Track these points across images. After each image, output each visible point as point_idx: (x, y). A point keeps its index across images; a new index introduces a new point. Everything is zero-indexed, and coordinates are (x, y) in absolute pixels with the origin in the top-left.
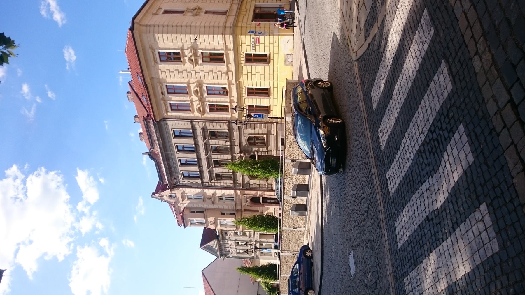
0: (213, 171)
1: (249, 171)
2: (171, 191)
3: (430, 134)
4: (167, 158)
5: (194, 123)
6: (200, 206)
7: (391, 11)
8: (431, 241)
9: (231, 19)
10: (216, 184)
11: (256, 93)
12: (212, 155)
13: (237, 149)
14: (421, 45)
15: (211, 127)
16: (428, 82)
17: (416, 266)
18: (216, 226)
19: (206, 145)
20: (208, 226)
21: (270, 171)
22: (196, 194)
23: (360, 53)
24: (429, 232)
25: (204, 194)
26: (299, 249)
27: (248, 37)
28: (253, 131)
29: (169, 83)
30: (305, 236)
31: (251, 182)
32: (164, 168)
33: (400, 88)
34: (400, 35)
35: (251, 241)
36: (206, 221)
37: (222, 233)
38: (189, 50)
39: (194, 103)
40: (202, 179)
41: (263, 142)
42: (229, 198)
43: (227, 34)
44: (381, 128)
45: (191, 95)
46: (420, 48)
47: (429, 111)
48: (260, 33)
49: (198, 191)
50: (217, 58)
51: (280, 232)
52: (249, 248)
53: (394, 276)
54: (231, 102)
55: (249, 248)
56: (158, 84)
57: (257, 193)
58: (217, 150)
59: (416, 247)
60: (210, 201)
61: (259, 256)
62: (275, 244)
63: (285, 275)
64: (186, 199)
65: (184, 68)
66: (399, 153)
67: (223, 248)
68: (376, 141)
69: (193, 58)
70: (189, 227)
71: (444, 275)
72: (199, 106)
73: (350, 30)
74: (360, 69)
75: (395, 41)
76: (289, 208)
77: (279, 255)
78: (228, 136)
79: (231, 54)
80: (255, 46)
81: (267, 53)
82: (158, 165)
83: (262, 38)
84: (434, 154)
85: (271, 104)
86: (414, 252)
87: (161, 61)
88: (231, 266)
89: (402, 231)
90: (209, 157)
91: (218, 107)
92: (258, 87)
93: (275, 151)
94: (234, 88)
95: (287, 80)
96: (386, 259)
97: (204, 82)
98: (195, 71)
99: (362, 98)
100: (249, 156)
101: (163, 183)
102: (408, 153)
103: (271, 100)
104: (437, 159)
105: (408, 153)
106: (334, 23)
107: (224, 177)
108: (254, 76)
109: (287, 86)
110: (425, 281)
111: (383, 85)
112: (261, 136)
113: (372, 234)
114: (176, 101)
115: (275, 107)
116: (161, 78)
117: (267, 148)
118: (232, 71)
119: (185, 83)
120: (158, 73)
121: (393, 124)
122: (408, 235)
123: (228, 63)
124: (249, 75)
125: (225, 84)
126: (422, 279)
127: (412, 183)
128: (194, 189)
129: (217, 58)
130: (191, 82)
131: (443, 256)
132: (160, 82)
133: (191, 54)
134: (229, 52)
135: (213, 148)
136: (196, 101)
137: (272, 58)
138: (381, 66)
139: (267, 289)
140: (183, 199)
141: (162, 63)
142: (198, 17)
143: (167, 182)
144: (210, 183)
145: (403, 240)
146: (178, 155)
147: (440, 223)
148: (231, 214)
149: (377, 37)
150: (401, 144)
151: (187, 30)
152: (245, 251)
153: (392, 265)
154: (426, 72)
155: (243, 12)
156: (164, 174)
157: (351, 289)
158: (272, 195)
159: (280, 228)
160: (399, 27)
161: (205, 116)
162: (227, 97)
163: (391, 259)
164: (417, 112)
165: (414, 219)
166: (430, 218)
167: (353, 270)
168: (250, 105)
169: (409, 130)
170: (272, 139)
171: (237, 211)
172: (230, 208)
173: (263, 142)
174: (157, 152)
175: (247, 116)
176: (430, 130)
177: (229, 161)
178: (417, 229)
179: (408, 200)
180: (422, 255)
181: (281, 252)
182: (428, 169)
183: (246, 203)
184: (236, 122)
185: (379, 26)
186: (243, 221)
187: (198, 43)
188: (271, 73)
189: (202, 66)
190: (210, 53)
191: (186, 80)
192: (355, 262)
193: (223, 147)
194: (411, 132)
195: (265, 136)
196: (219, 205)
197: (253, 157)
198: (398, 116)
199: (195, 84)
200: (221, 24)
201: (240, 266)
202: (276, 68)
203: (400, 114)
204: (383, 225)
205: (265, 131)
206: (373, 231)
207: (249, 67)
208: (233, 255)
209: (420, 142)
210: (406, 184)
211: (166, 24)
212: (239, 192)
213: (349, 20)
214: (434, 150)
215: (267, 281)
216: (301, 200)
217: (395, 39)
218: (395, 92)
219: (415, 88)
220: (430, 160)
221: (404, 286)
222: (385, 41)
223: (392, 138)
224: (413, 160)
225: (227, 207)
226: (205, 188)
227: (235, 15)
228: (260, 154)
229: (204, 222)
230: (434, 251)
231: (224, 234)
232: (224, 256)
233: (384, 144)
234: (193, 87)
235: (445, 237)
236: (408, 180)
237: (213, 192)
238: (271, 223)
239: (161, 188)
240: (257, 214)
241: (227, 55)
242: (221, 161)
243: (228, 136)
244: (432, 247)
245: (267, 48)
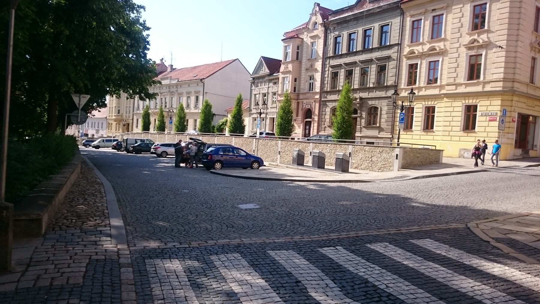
0: (341, 69)
1: (341, 107)
2: (321, 24)
3: (386, 294)
4: (357, 18)
5: (396, 48)
6: (304, 55)
7: (531, 269)
8: (277, 282)
9: (523, 89)
10: (327, 72)
11: (428, 116)
12: (359, 68)
13: (364, 95)
14: (489, 297)
15: (391, 67)
16: (445, 299)
17: (252, 265)
18: (283, 73)
19: (370, 61)
20: (284, 64)
21: (339, 130)
22: (317, 51)
23: (477, 231)
24: (285, 282)
25: (316, 60)
26: (259, 156)
27: (499, 108)
28: (384, 112)
29: (446, 17)
30: (272, 163)
31: (328, 110)
32: (346, 15)
33: (436, 270)
34: (501, 276)
35: (267, 108)
36: (289, 63)
37: (276, 79)
38: (487, 40)
39: (420, 47)
40: (332, 57)
41: (371, 123)
42: (311, 87)
43: (503, 84)
44: (389, 245)
45: (430, 43)
46: (486, 296)
47: (412, 296)
48: (502, 122)
49: (321, 53)
50: (474, 72)
51: (276, 138)
52: (261, 106)
53: (240, 244)
54: (420, 89)
55: (261, 106)
56: (445, 5)
57: (316, 116)
58: (364, 73)
59: (269, 268)
60: (309, 66)
61: (252, 116)
62: (264, 133)
63: (235, 142)
64: (312, 41)
65: (464, 34)
66: (364, 261)
67: (261, 80)
68: (377, 239)
69: (476, 44)
70: (282, 44)
71: (246, 291)
72: (416, 52)
73: (504, 222)
74: (456, 230)
75: (492, 270)
76: (300, 148)
77: (253, 136)
78: (380, 85)
79: (479, 89)
80: (486, 115)
81: (477, 129)
82: (351, 8)
83: (496, 124)
84: (365, 296)
85: (415, 133)
86: (264, 265)
87: (475, 6)
88: (243, 88)
89: (284, 256)
90: (357, 65)
91: (414, 73)
92: (436, 119)
93: (360, 135)
94: (436, 92)
95: (442, 151)
96: (256, 239)
97: (445, 58)
98: (460, 47)
99: (423, 229)
100: (357, 108)
101: (330, 15)
102: (364, 270)
103: (419, 133)
104: (360, 298)
105: (364, 270)
106: (513, 206)
107: (335, 80)
108: (449, 114)
109: (435, 150)
110: (238, 273)
111: (439, 252)
112: (378, 121)
113: (279, 228)
114: (424, 26)
115: (410, 137)
116: (453, 7)
117: (364, 127)
118: (456, 89)
119: (445, 35)
120: (459, 4)
121: (395, 258)
122: (280, 261)
123: (467, 85)
124: (451, 109)
125: (441, 82)
126: (240, 270)
127: (333, 270)
128: (322, 49)
129: (474, 72)
130: (445, 43)
131: (262, 292)
132: (448, 7)
133: (481, 41)
134: (481, 86)
135: (367, 69)
136: (423, 49)
137: (470, 134)
138: (462, 252)
139: (221, 124)
140: (311, 37)
141: (411, 22)
142: (529, 49)
143: (332, 19)
144: (328, 66)
145: (275, 256)
146: (360, 30)
147: (294, 293)
148: (295, 88)
149: (498, 251)
150: (374, 264)
151: (513, 36)
152: (264, 102)
153: (250, 244)
154: (456, 299)
155: (531, 102)
156: (339, 15)
157: (225, 204)
158: (314, 131)
159: (280, 138)
160: (511, 275)
161: (405, 59)
162: (426, 83)
163: (256, 243)
164: (410, 284)
165: (296, 269)
166: (299, 284)
167: (243, 206)
168: (415, 109)
169: (389, 274)
170: (374, 133)
171: (298, 95)
172: (301, 87)
173: (371, 123)
174: (365, 6)
175: (403, 106)
176: (390, 295)
177: (351, 86)
178: (287, 270)
179: (316, 265)
180: (262, 272)
181: (256, 139)
182: (349, 288)
183: (305, 104)
184: (396, 93)
185: (511, 254)
186: (288, 101)
187: (494, 50)
188: (451, 133)
189: (465, 55)
190: (481, 64)
191: (448, 37)
192: (250, 209)
193: (367, 79)
194: (387, 276)
195: (378, 125)
196: (304, 76)
197: (355, 112)
198: (404, 264)
199: (443, 47)
200: (517, 77)
201: (243, 97)
202: (457, 139)
203: (407, 267)
204: (288, 239)
205: (384, 125)
206: (282, 229)
207: (460, 109)
208: (253, 91)
209: (376, 283)
210: (332, 265)
211: (523, 10)
212: (317, 97)
213: (517, 222)
214: (368, 296)
215: (228, 124)
216: (309, 161)
217: (495, 270)
218: (431, 263)
219: (438, 285)
220: (358, 291)
221: (232, 252)
222: (492, 259)
223: (379, 255)
224: (357, 274)
225: (302, 84)
226: (323, 61)
227: (527, 93)
228: (358, 119)
229: (287, 60)
230: (267, 284)
231: (275, 81)
232: (253, 81)
233: (372, 247)
234: (439, 45)
235: (282, 296)
236: (336, 267)
237: (318, 69)
238: (285, 130)
239: (325, 13)
240: (294, 115)
241: (478, 84)
242: (352, 78)
243: (380, 85)
244: (271, 283)
245: (482, 129)
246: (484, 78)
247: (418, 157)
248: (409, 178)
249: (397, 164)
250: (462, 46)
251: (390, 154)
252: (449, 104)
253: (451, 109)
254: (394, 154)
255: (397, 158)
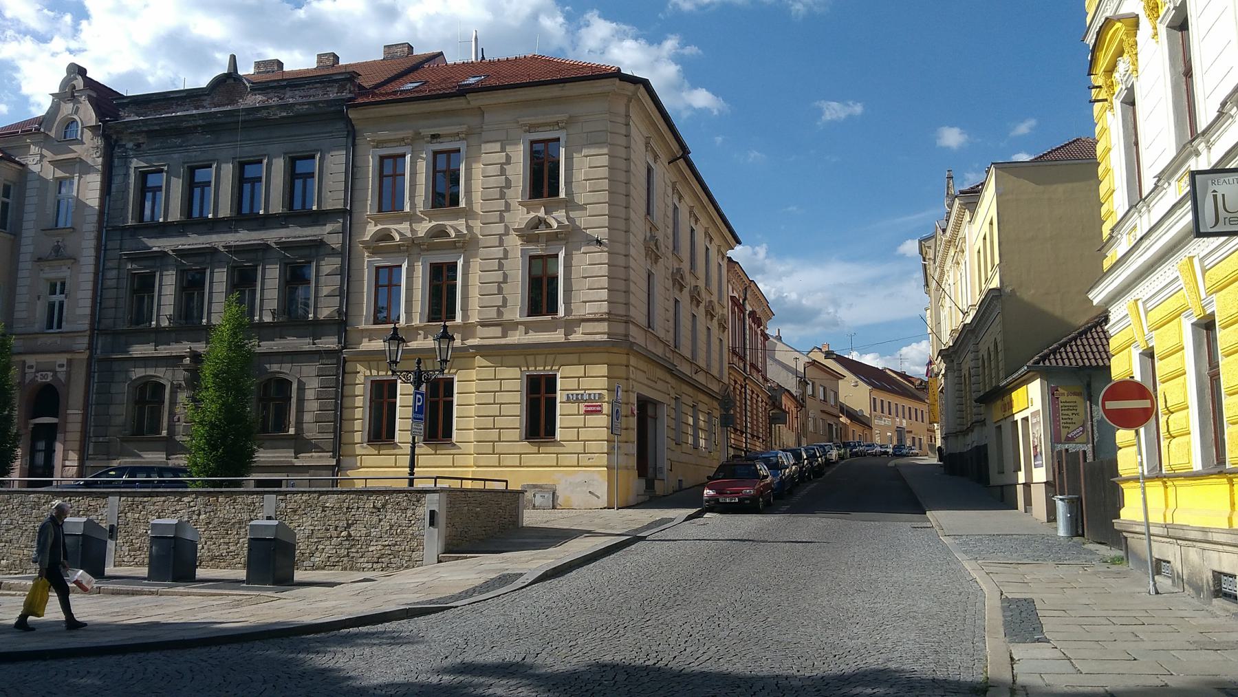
2: (93, 129)
21: (214, 447)
27: (604, 383)
28: (310, 394)
42: (55, 316)
50: (542, 294)
56: (464, 128)
64: (59, 174)
65: (514, 203)
69: (542, 230)
78: (293, 318)
79: (558, 336)
80: (577, 401)
81: (559, 435)
83: (602, 420)
112: (293, 418)
118: (504, 335)
123: (528, 327)
129: (542, 294)
141: (377, 159)
172: (17, 315)
191: (477, 208)
195: (292, 431)
205: (312, 432)
234: (455, 226)
239: (105, 100)
241: (551, 327)
246: (568, 311)
247: (477, 515)
248: (519, 583)
249: (433, 541)
250: (512, 232)
251: (409, 513)
252: (489, 373)
253: (495, 385)
254: (423, 511)
255: (432, 524)
